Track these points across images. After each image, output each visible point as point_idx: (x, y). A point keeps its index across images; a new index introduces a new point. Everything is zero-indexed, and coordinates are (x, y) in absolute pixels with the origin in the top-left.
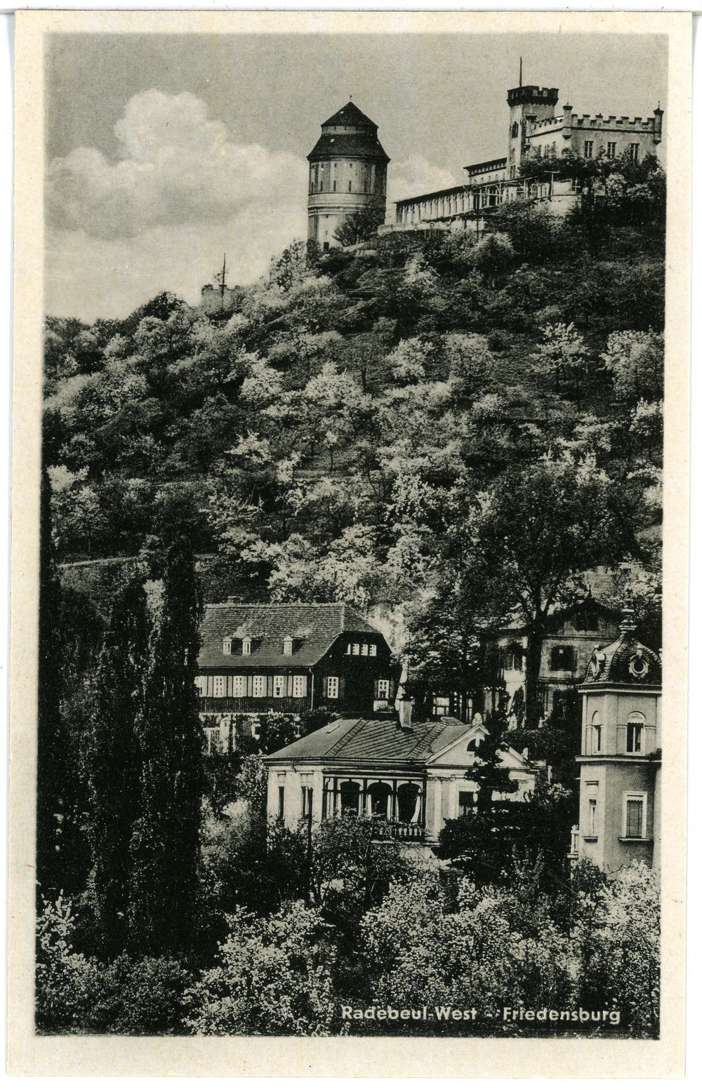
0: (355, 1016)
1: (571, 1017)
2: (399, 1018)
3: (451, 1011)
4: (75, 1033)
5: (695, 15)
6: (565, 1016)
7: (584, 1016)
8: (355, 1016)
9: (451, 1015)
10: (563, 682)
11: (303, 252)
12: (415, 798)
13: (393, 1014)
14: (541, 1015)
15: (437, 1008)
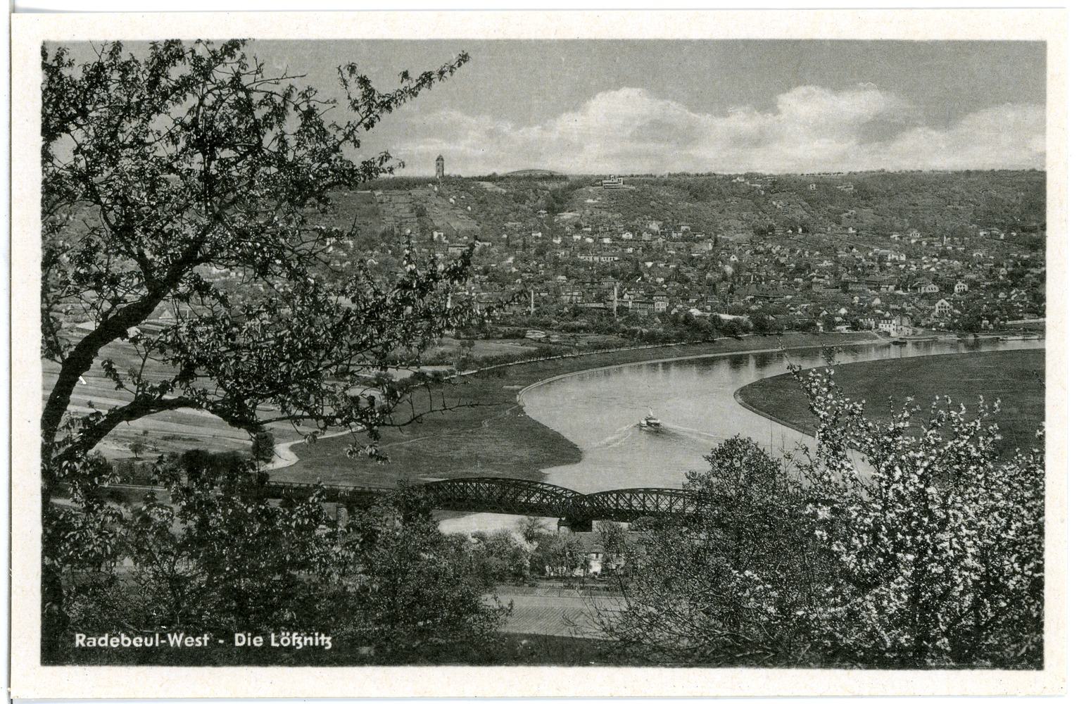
0: (88, 644)
1: (195, 642)
2: (132, 645)
3: (184, 638)
4: (860, 668)
5: (14, 10)
6: (308, 641)
7: (126, 642)
8: (88, 644)
9: (183, 644)
10: (868, 347)
11: (109, 49)
12: (165, 400)
13: (126, 642)
14: (103, 642)
15: (169, 635)
